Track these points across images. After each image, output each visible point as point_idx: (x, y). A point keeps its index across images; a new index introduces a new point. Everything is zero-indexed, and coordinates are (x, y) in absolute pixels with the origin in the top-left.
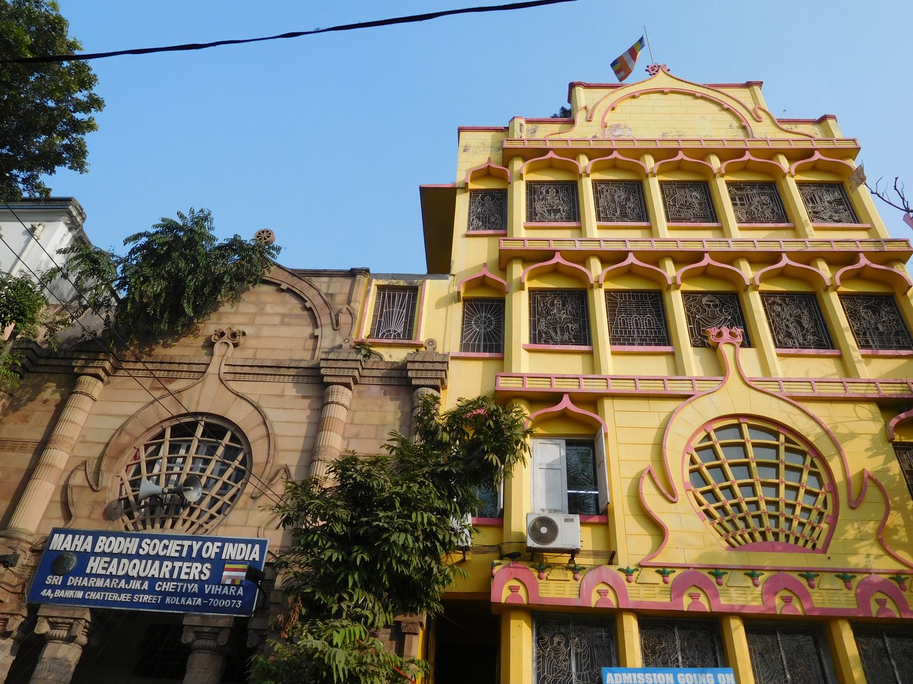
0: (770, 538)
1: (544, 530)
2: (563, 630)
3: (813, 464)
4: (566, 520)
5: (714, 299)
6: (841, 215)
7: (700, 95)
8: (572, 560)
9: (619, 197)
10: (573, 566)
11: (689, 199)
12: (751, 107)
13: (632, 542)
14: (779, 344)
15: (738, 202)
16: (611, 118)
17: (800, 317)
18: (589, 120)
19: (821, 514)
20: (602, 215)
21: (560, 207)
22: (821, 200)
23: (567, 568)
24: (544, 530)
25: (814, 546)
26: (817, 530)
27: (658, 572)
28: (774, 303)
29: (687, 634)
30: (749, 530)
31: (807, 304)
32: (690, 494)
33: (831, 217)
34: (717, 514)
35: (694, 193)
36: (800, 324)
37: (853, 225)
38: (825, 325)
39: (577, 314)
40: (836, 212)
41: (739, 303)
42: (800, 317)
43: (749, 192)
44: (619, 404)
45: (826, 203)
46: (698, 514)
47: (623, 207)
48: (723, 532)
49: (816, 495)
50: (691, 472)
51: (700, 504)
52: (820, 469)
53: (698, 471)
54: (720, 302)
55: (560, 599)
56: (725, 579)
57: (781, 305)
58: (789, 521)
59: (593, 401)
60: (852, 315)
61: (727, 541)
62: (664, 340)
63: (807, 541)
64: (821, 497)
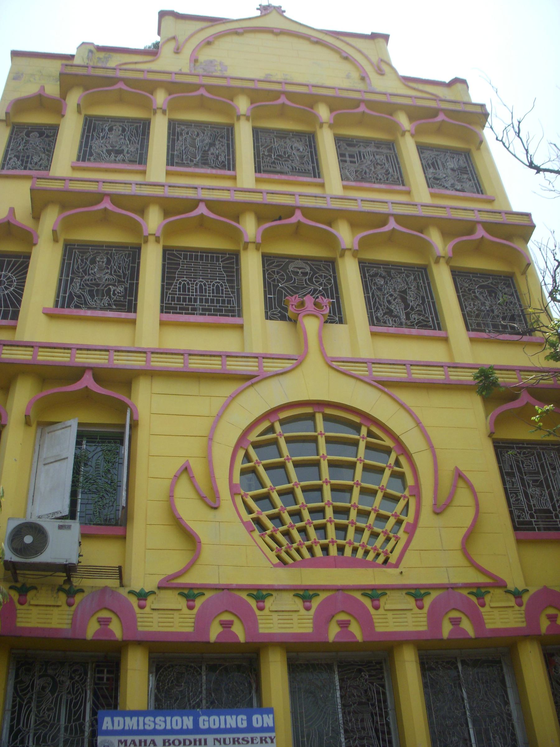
0: (319, 552)
1: (28, 539)
2: (50, 672)
3: (397, 463)
4: (61, 527)
5: (304, 265)
6: (464, 185)
7: (315, 40)
8: (68, 581)
9: (203, 141)
10: (67, 587)
11: (289, 150)
12: (375, 60)
13: (149, 555)
14: (373, 320)
15: (348, 159)
16: (205, 56)
17: (405, 292)
18: (177, 51)
19: (399, 522)
20: (176, 160)
21: (124, 147)
22: (444, 166)
23: (60, 589)
24: (28, 539)
25: (386, 561)
26: (392, 542)
27: (181, 594)
28: (376, 275)
29: (209, 673)
30: (308, 543)
31: (415, 279)
32: (239, 500)
33: (453, 186)
34: (269, 524)
35: (296, 145)
36: (404, 300)
37: (476, 195)
38: (434, 303)
39: (125, 275)
40: (459, 181)
41: (334, 272)
42: (405, 292)
43: (362, 149)
44: (159, 386)
45: (449, 171)
46: (246, 524)
47: (205, 153)
48: (274, 545)
49: (396, 500)
50: (243, 472)
51: (250, 511)
52: (406, 468)
53: (253, 471)
54: (311, 269)
55: (43, 629)
56: (269, 603)
57: (384, 278)
58: (321, 528)
59: (126, 379)
60: (463, 295)
61: (278, 557)
62: (233, 311)
63: (378, 555)
64: (402, 503)
